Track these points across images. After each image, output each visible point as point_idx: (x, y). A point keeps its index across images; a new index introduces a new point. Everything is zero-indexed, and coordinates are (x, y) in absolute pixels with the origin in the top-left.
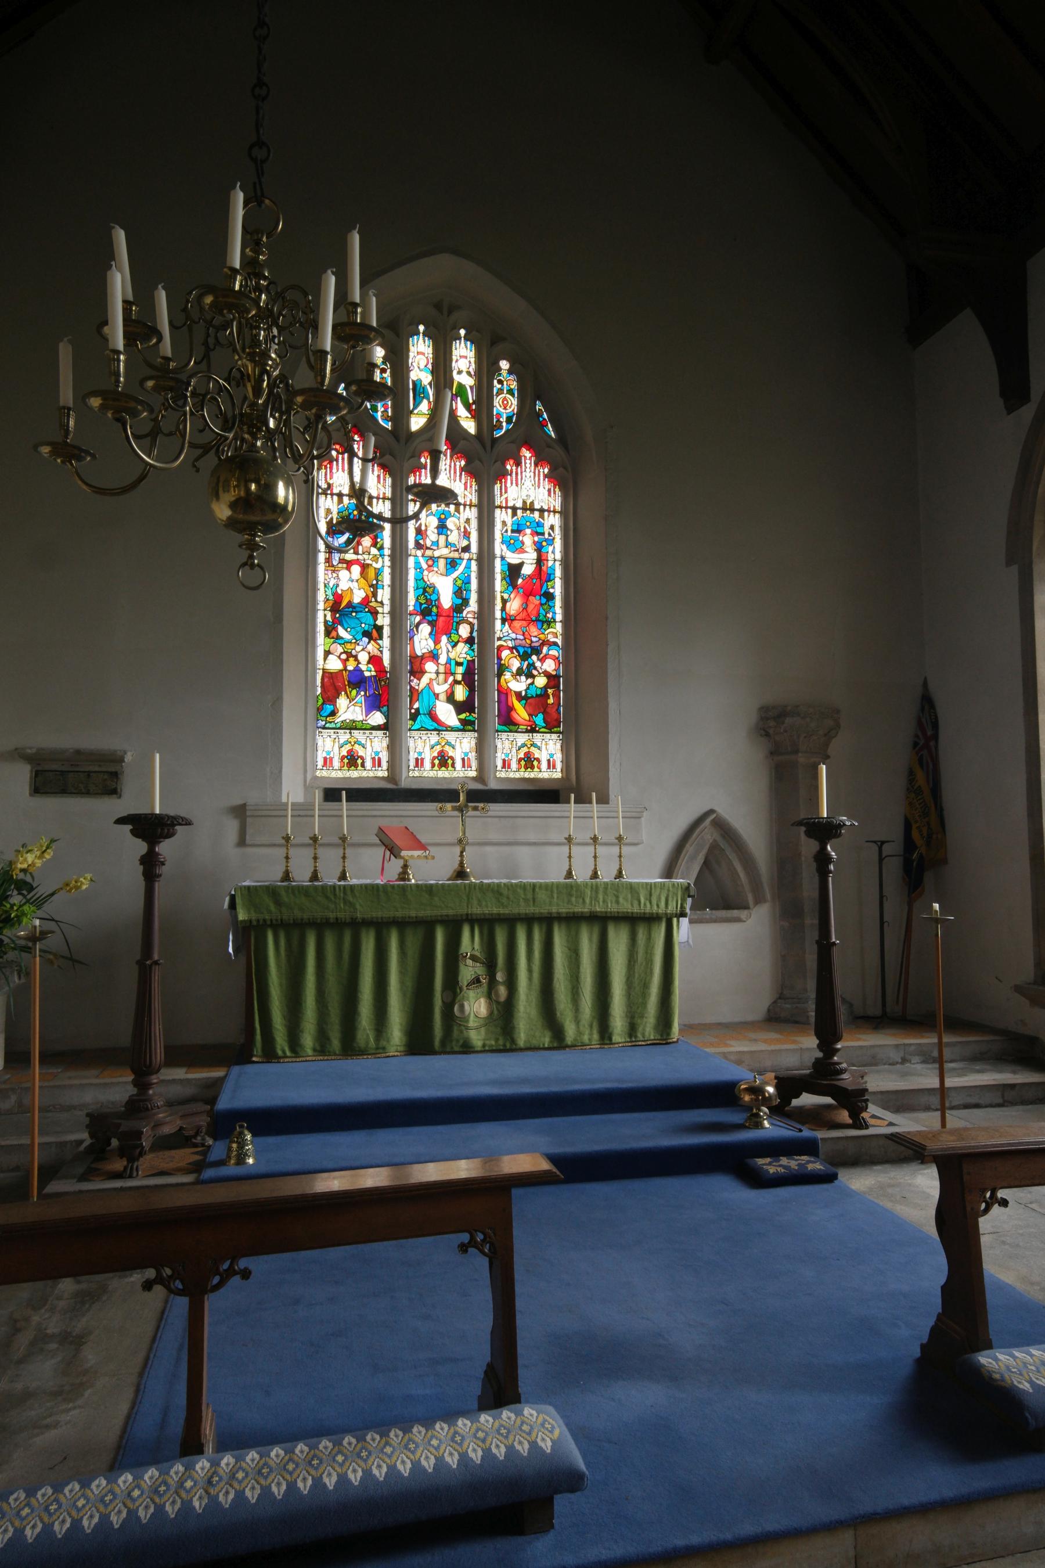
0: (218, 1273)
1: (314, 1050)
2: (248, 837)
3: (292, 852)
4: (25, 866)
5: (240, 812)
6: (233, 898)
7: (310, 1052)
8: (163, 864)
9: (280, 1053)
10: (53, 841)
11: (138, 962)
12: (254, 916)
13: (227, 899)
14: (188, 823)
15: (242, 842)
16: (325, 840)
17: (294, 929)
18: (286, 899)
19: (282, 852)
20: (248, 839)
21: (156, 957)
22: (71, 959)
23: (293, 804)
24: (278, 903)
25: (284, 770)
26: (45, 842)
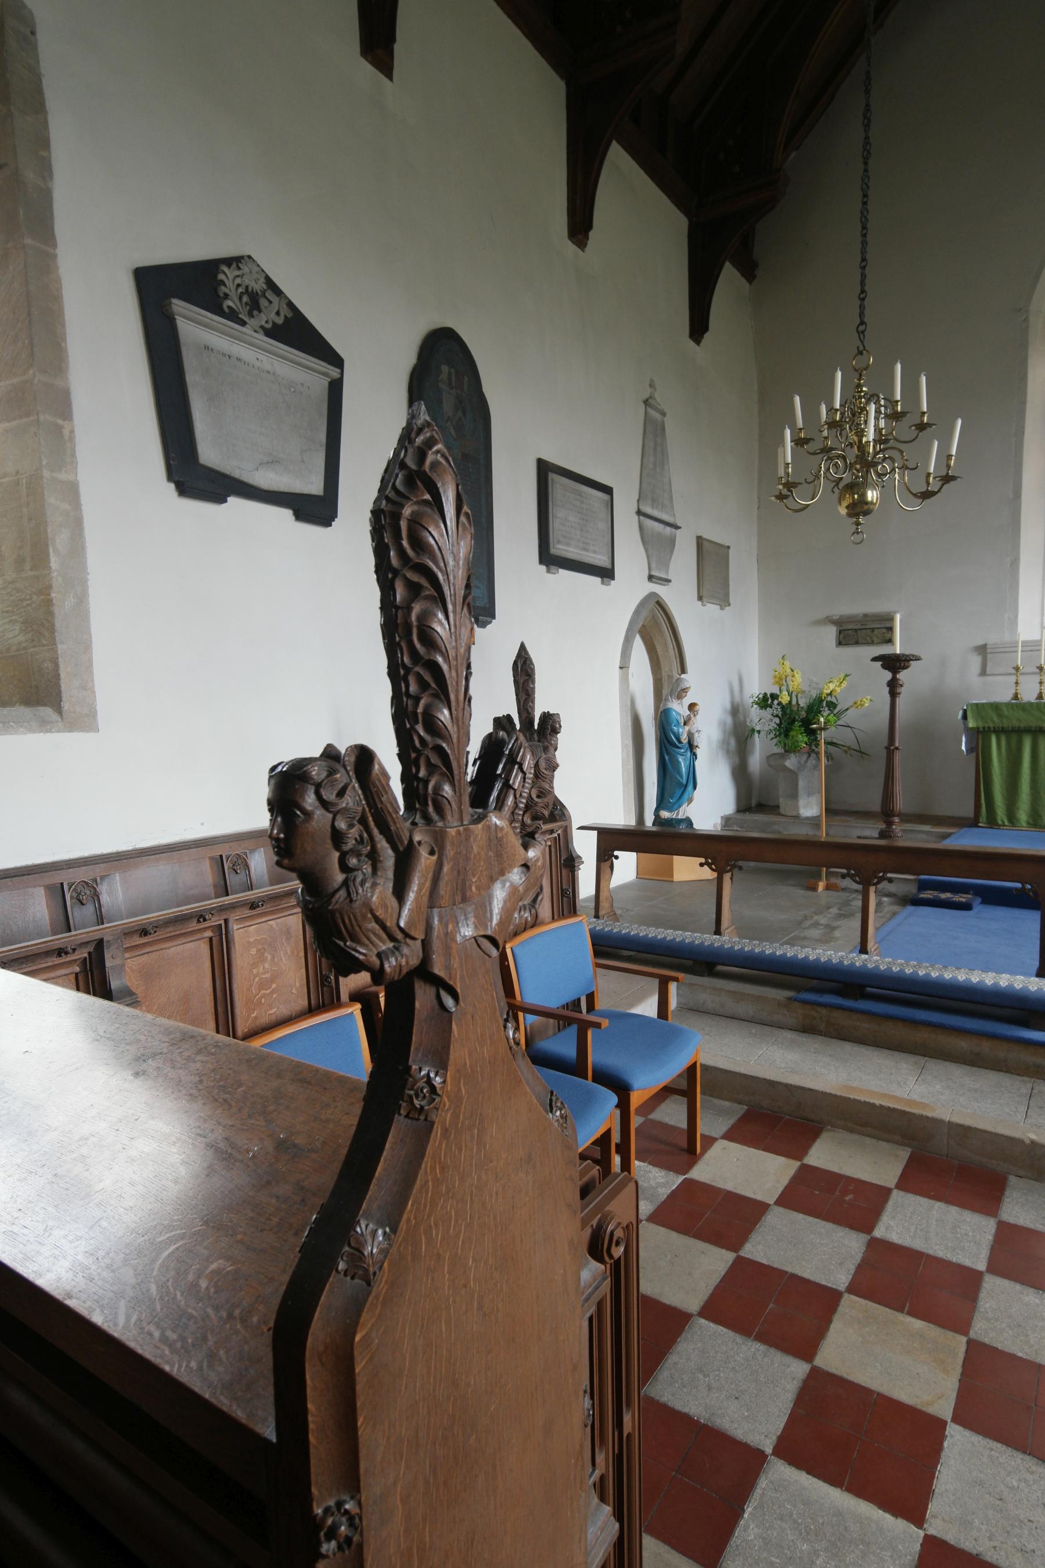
0: (876, 877)
1: (1028, 823)
2: (988, 669)
3: (1021, 679)
4: (829, 691)
5: (982, 650)
6: (965, 711)
7: (1024, 824)
8: (901, 686)
9: (1000, 822)
10: (846, 676)
11: (887, 748)
12: (981, 725)
13: (961, 713)
14: (918, 659)
15: (983, 673)
16: (1026, 670)
17: (1013, 734)
18: (1006, 713)
19: (1013, 679)
20: (988, 670)
21: (897, 745)
22: (860, 752)
23: (1023, 642)
24: (1000, 715)
25: (1020, 616)
26: (842, 676)
